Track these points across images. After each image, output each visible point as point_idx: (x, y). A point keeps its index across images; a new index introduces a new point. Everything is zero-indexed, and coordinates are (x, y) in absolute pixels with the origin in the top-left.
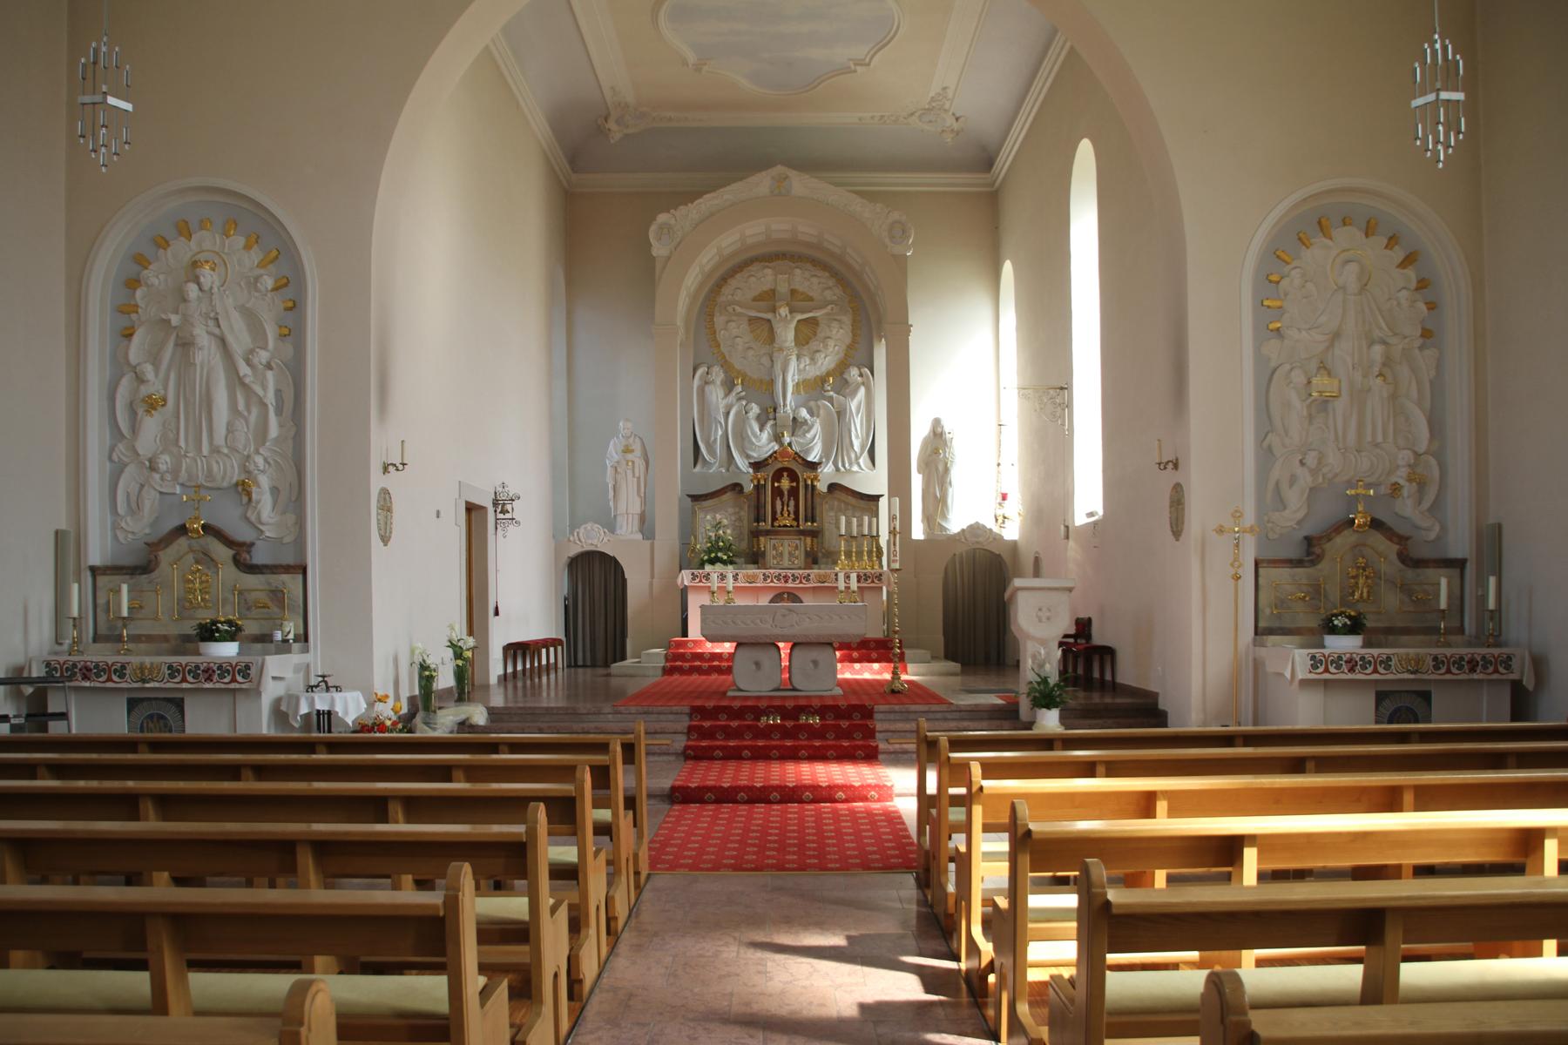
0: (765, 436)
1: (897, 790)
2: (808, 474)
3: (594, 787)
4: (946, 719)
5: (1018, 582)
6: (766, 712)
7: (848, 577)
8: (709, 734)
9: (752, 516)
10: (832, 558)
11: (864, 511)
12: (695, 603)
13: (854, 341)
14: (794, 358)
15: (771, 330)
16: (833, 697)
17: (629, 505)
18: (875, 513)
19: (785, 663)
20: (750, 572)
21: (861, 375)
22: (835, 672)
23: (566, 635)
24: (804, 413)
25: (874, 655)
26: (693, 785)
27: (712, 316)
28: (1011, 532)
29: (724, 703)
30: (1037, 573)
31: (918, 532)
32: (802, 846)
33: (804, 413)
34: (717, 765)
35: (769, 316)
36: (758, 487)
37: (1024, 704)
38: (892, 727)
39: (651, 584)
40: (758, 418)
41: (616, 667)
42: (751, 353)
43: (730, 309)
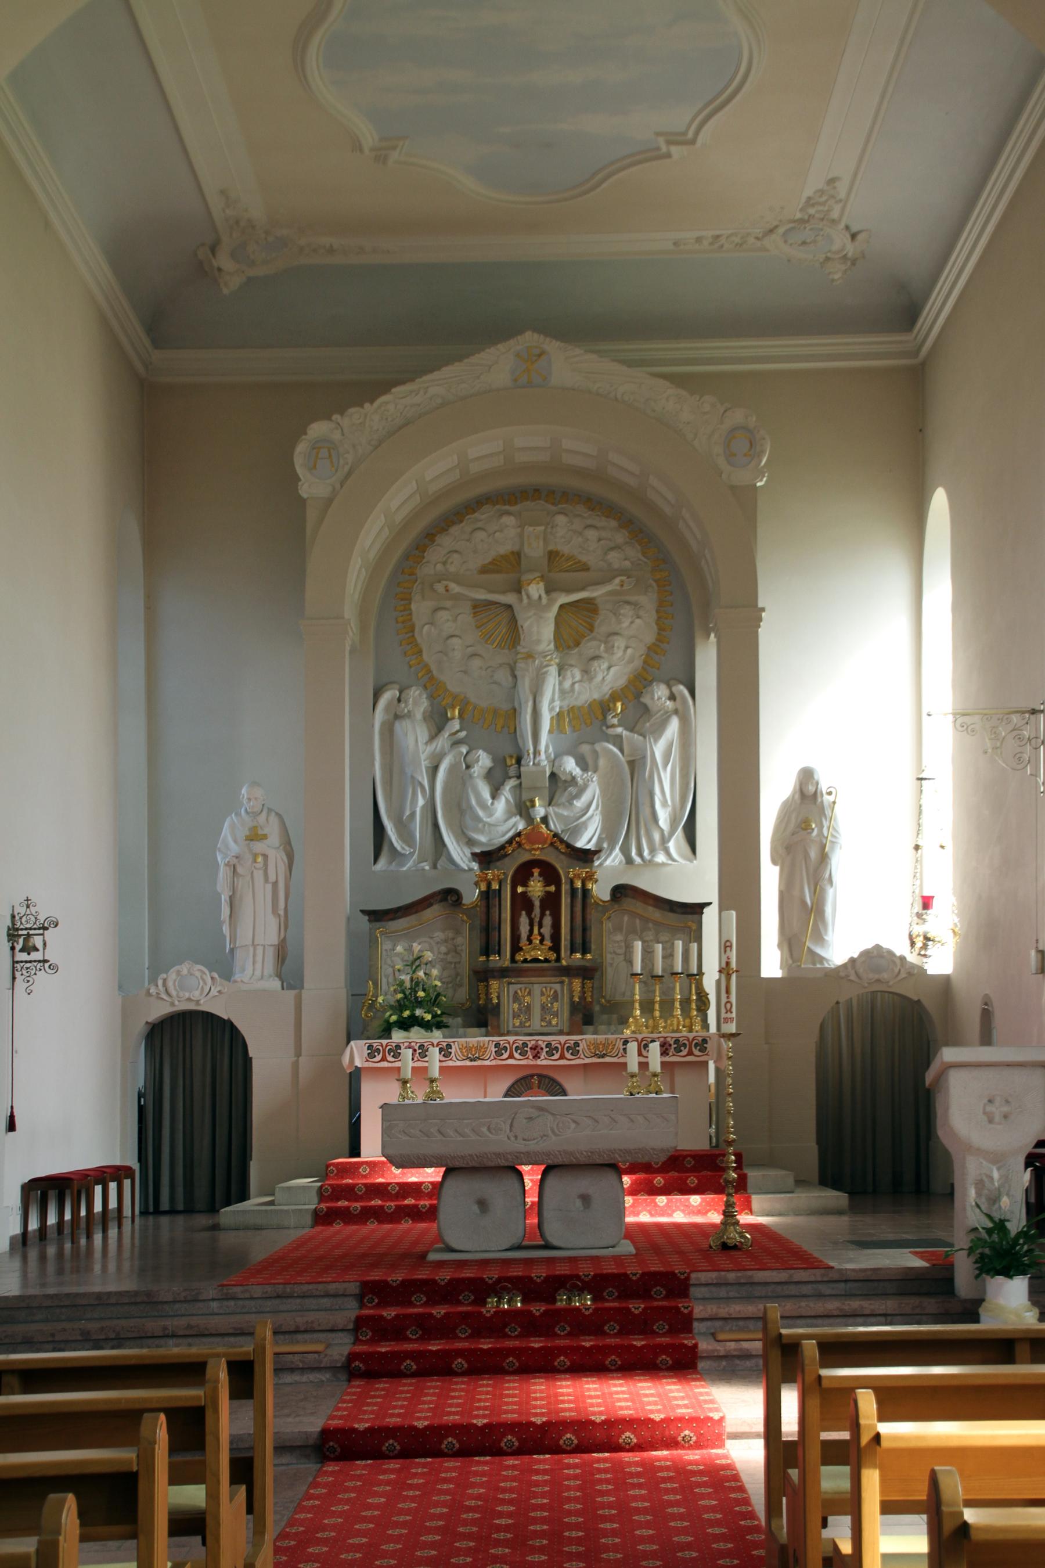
0: (501, 806)
1: (729, 1427)
3: (173, 1450)
4: (820, 1296)
5: (949, 1054)
6: (497, 1288)
8: (394, 1331)
9: (477, 945)
10: (617, 1013)
11: (675, 931)
12: (376, 1097)
13: (660, 639)
14: (553, 670)
15: (513, 623)
16: (618, 1259)
17: (257, 929)
18: (697, 936)
19: (531, 1199)
20: (473, 1041)
21: (672, 697)
22: (621, 1212)
23: (141, 1159)
24: (570, 765)
25: (692, 1181)
26: (361, 1426)
28: (941, 962)
29: (422, 1274)
30: (986, 1039)
31: (771, 965)
32: (556, 1536)
33: (570, 765)
34: (407, 1386)
35: (509, 598)
37: (964, 1268)
38: (724, 1311)
39: (296, 1066)
40: (489, 775)
41: (229, 1213)
42: (476, 663)
43: (440, 588)
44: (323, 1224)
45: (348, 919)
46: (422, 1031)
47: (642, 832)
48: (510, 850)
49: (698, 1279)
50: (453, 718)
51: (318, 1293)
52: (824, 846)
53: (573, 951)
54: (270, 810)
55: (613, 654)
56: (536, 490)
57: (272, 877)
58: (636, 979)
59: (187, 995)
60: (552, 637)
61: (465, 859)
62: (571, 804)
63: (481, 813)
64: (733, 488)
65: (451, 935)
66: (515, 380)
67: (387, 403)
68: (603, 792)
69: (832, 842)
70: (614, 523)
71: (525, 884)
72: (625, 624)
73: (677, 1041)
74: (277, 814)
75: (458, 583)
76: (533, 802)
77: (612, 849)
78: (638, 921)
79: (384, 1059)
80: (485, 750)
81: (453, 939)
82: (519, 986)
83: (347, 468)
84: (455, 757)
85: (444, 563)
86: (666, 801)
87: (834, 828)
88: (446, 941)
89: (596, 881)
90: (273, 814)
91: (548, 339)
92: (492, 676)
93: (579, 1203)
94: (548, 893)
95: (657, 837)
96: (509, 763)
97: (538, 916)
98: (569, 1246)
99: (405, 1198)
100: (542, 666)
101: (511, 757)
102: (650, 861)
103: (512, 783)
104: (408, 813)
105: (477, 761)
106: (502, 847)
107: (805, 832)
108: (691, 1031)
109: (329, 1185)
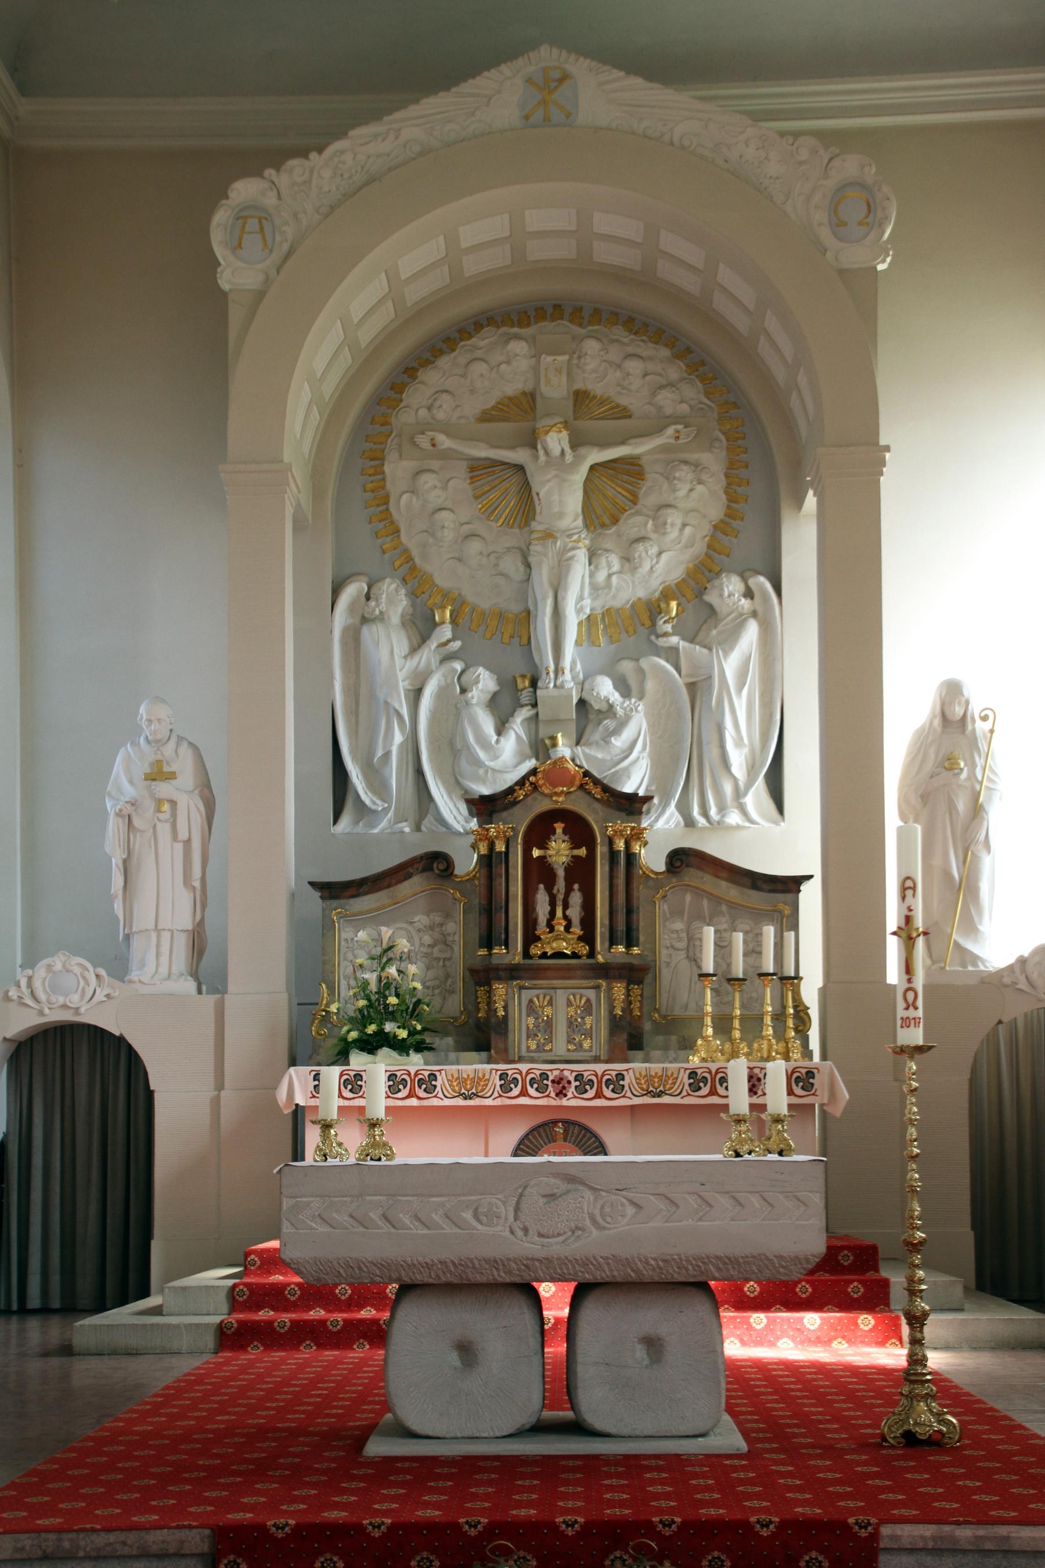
2: (619, 825)
7: (755, 1084)
9: (475, 934)
10: (680, 1034)
11: (760, 916)
13: (731, 514)
14: (581, 556)
17: (162, 908)
21: (749, 594)
24: (605, 688)
27: (378, 458)
33: (605, 688)
35: (519, 456)
36: (488, 861)
40: (493, 703)
42: (475, 546)
43: (423, 441)
44: (231, 1349)
45: (293, 895)
46: (394, 1054)
47: (708, 782)
48: (521, 794)
49: (894, 1538)
50: (443, 623)
51: (126, 1551)
52: (976, 795)
53: (613, 942)
54: (180, 739)
55: (665, 534)
56: (557, 307)
57: (183, 835)
59: (61, 1000)
60: (580, 510)
61: (459, 818)
62: (607, 743)
63: (482, 755)
64: (841, 272)
65: (438, 919)
66: (527, 117)
67: (342, 152)
68: (652, 726)
69: (988, 788)
70: (665, 352)
71: (543, 846)
72: (681, 493)
74: (190, 743)
75: (448, 435)
76: (553, 739)
77: (665, 805)
80: (487, 668)
81: (441, 925)
82: (536, 992)
83: (285, 247)
84: (445, 676)
85: (429, 408)
86: (741, 739)
87: (991, 769)
88: (431, 928)
89: (646, 844)
90: (185, 744)
91: (573, 57)
92: (497, 565)
93: (640, 1352)
94: (575, 858)
95: (728, 788)
96: (520, 686)
97: (563, 890)
98: (625, 1431)
99: (361, 1307)
100: (565, 550)
101: (523, 677)
102: (718, 823)
103: (525, 713)
104: (380, 753)
105: (477, 682)
106: (510, 791)
107: (951, 773)
109: (245, 1285)
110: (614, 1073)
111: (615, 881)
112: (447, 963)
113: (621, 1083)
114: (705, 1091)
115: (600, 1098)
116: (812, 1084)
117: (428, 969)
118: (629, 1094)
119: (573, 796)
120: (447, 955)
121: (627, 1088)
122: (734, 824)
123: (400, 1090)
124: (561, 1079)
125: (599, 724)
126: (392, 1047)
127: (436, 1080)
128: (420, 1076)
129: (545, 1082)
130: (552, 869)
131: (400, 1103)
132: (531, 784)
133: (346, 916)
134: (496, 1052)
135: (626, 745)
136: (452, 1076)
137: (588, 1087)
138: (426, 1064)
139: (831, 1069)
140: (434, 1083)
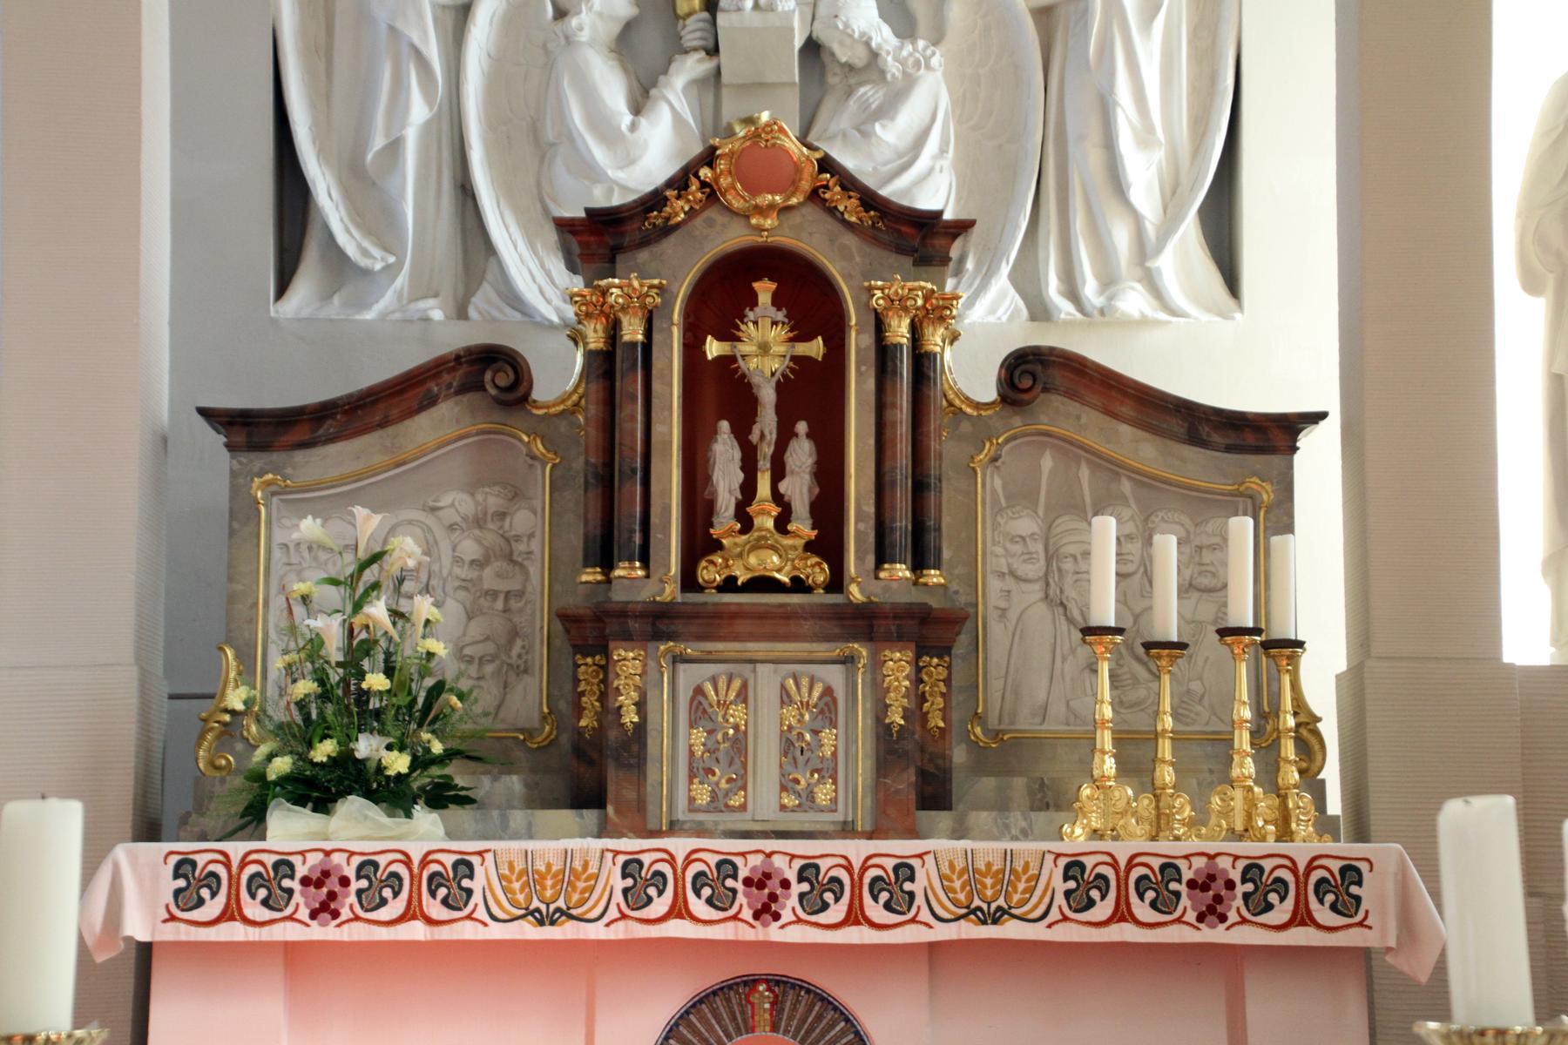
9: (575, 540)
18: (1277, 516)
36: (607, 365)
40: (624, 43)
46: (375, 812)
47: (1079, 224)
48: (678, 208)
53: (883, 556)
58: (1101, 646)
61: (550, 291)
63: (599, 154)
65: (494, 502)
71: (728, 334)
73: (1252, 871)
77: (988, 275)
78: (1085, 473)
79: (231, 913)
81: (502, 515)
82: (711, 669)
86: (1150, 129)
88: (479, 522)
89: (954, 338)
95: (1121, 237)
97: (771, 436)
102: (1102, 312)
103: (691, 67)
104: (378, 142)
106: (655, 200)
108: (1285, 834)
110: (890, 863)
111: (888, 414)
112: (513, 604)
113: (907, 886)
114: (1103, 910)
115: (857, 923)
116: (1358, 899)
117: (470, 618)
118: (925, 915)
119: (796, 218)
120: (515, 585)
121: (919, 900)
122: (1136, 315)
123: (383, 902)
124: (768, 876)
125: (849, 93)
126: (370, 795)
127: (471, 877)
128: (435, 867)
129: (730, 883)
130: (749, 386)
131: (384, 934)
132: (704, 184)
133: (286, 490)
134: (617, 811)
135: (908, 139)
136: (511, 867)
137: (828, 897)
138: (451, 835)
139: (1401, 855)
140: (466, 883)
